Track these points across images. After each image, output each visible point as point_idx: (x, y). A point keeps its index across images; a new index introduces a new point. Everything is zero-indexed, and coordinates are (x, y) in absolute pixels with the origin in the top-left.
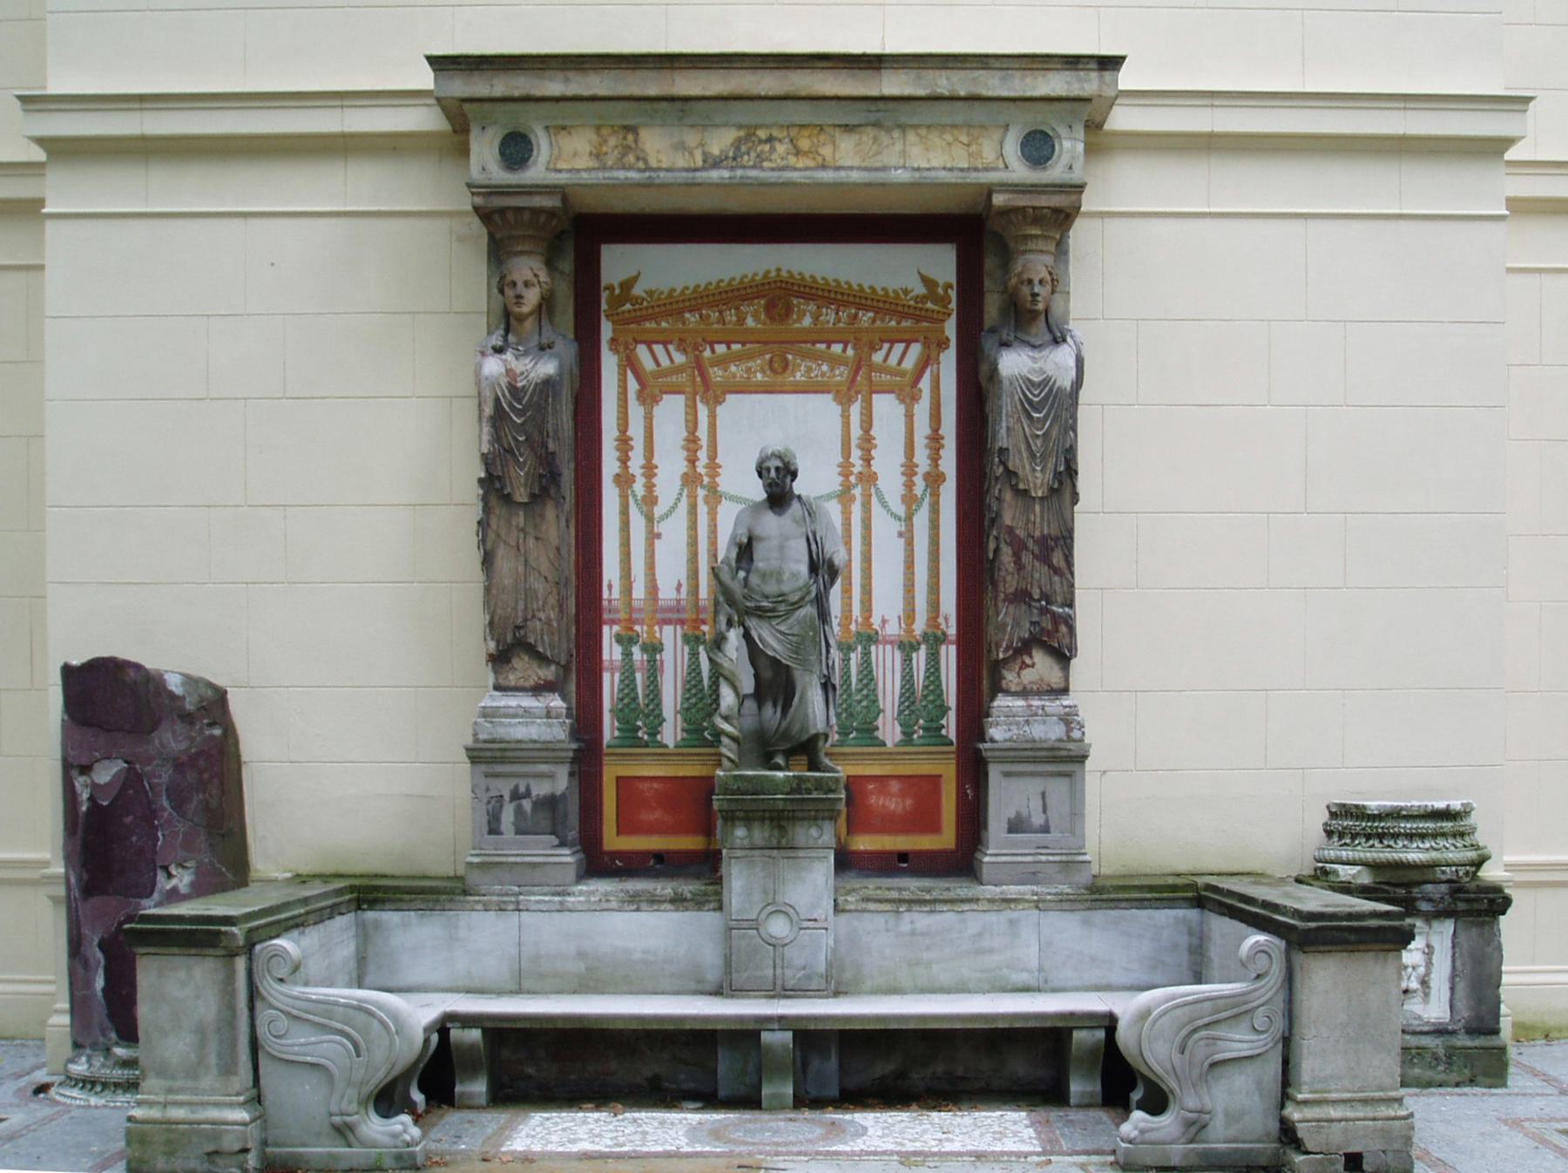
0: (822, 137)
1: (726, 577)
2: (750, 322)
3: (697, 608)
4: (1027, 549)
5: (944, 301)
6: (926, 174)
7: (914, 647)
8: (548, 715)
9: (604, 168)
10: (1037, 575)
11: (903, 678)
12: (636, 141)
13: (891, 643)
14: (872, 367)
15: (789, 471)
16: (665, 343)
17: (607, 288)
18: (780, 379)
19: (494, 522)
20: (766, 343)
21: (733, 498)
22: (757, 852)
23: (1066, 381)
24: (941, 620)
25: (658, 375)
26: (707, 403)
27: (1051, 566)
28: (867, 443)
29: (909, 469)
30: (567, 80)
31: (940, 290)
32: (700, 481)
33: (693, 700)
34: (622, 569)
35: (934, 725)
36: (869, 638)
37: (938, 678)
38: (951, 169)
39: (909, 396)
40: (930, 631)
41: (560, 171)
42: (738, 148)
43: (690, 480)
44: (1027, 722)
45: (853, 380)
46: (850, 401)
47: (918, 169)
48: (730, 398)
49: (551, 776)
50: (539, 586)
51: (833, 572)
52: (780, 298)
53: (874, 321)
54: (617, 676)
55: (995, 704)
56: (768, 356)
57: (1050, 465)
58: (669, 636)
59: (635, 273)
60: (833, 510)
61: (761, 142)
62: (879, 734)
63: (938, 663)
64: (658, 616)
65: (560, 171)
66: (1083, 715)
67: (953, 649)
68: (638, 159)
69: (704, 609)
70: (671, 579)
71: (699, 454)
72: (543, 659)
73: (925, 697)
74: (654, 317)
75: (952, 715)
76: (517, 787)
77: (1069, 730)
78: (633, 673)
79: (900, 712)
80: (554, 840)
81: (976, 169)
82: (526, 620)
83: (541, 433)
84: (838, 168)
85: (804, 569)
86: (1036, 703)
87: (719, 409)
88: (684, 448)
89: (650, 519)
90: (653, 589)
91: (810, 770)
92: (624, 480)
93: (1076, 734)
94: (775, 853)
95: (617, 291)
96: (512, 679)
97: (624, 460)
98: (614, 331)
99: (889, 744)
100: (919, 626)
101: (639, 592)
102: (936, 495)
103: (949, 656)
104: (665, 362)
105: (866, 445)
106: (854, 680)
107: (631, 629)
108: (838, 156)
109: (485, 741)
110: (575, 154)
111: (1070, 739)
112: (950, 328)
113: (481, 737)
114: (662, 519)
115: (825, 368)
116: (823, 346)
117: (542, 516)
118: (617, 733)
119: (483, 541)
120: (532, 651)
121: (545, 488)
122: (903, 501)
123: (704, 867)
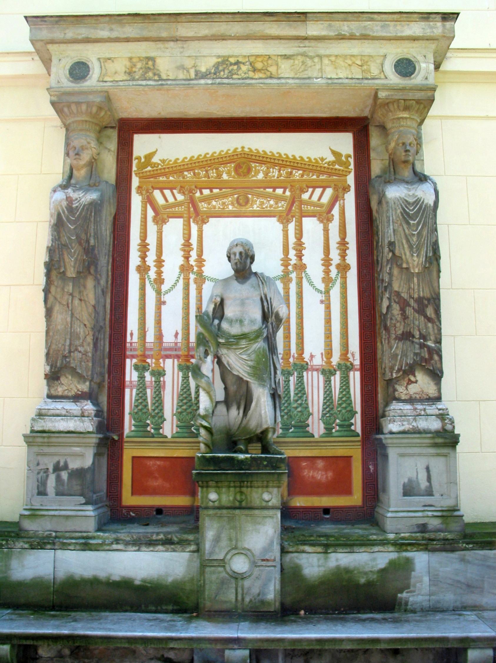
2: (225, 177)
3: (189, 349)
4: (409, 306)
5: (346, 164)
7: (332, 373)
9: (134, 80)
10: (417, 323)
11: (325, 392)
12: (154, 65)
13: (317, 370)
14: (302, 202)
16: (171, 189)
17: (136, 158)
18: (243, 209)
19: (53, 289)
20: (235, 188)
21: (212, 280)
22: (225, 511)
23: (430, 200)
24: (349, 355)
25: (165, 207)
26: (197, 223)
27: (426, 317)
28: (300, 247)
29: (327, 262)
30: (111, 30)
31: (343, 158)
32: (192, 269)
33: (184, 407)
34: (140, 324)
35: (347, 423)
36: (302, 367)
37: (349, 392)
38: (352, 79)
39: (325, 217)
40: (342, 362)
41: (106, 82)
42: (217, 68)
43: (185, 269)
44: (415, 420)
45: (290, 210)
46: (288, 221)
47: (330, 79)
49: (82, 455)
50: (80, 330)
51: (279, 320)
52: (244, 163)
53: (302, 176)
54: (134, 391)
55: (392, 408)
56: (236, 196)
57: (423, 253)
58: (170, 366)
59: (154, 150)
60: (280, 286)
61: (231, 64)
62: (310, 429)
64: (163, 353)
65: (106, 82)
66: (452, 414)
67: (358, 374)
70: (172, 327)
71: (191, 253)
72: (81, 378)
73: (340, 405)
74: (165, 174)
75: (358, 417)
76: (58, 462)
78: (145, 389)
79: (324, 415)
80: (82, 500)
81: (367, 79)
82: (70, 352)
83: (86, 234)
84: (279, 78)
85: (258, 315)
86: (419, 407)
87: (205, 227)
89: (159, 292)
90: (159, 336)
91: (262, 453)
92: (143, 269)
93: (449, 427)
95: (143, 160)
96: (60, 390)
97: (143, 257)
98: (140, 182)
99: (316, 436)
100: (335, 359)
101: (150, 337)
102: (344, 278)
103: (355, 378)
104: (171, 200)
106: (292, 394)
107: (145, 361)
108: (279, 72)
110: (116, 73)
112: (351, 180)
113: (36, 428)
114: (166, 292)
115: (272, 202)
116: (271, 190)
117: (85, 287)
119: (46, 301)
120: (74, 372)
121: (89, 266)
123: (190, 519)
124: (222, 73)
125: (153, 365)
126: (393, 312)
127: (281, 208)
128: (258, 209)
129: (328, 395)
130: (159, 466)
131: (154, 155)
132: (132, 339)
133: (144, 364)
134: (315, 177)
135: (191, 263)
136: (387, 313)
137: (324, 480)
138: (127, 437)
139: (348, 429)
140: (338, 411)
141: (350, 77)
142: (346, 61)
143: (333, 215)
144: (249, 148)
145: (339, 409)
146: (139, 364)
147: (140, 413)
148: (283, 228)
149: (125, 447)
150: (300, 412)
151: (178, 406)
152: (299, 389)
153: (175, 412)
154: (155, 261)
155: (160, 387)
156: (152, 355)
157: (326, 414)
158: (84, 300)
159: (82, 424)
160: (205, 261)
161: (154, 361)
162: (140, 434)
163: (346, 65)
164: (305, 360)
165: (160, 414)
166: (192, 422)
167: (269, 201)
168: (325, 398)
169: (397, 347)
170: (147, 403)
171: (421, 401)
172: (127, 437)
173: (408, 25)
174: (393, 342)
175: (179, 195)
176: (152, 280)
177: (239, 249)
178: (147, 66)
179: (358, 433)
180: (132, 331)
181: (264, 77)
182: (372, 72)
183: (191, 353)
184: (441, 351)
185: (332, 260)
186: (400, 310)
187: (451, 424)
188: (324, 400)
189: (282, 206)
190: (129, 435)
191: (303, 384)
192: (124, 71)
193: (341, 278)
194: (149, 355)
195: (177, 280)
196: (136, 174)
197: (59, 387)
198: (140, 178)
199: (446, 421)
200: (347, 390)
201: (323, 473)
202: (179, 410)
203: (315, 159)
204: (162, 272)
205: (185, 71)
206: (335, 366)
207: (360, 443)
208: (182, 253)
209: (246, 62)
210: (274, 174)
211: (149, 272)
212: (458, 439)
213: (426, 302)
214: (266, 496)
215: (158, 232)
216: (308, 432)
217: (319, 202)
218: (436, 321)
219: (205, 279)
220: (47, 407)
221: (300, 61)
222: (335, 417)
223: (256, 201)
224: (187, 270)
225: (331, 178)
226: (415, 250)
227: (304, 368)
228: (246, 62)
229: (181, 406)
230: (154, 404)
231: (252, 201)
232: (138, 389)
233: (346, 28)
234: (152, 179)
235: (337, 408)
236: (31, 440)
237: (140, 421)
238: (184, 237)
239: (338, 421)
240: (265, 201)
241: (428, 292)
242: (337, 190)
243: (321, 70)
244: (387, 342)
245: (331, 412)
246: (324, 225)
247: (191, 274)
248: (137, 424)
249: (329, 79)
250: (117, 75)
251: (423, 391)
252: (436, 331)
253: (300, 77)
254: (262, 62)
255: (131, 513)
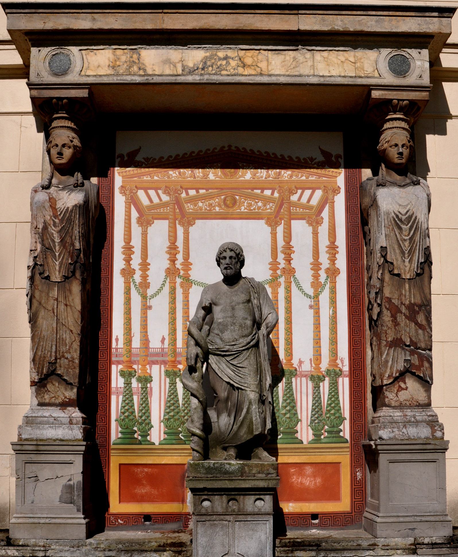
0: (260, 57)
1: (195, 331)
4: (401, 313)
6: (328, 79)
7: (321, 379)
8: (71, 423)
9: (118, 75)
11: (314, 399)
13: (305, 376)
14: (291, 204)
15: (239, 259)
16: (156, 189)
18: (231, 210)
19: (37, 294)
20: (222, 189)
21: (199, 284)
24: (339, 361)
25: (150, 208)
28: (288, 250)
29: (316, 266)
31: (333, 159)
32: (178, 273)
33: (172, 414)
34: (125, 329)
37: (338, 398)
38: (344, 77)
39: (314, 218)
40: (331, 368)
41: (88, 76)
43: (171, 272)
44: (405, 426)
45: (279, 211)
46: (277, 224)
47: (323, 76)
48: (199, 223)
50: (67, 336)
53: (291, 176)
54: (121, 398)
56: (223, 197)
58: (156, 372)
59: (137, 147)
61: (220, 59)
62: (298, 435)
63: (337, 389)
67: (347, 380)
68: (140, 69)
69: (180, 354)
70: (158, 333)
71: (177, 256)
75: (347, 424)
77: (433, 431)
78: (132, 395)
79: (312, 421)
81: (360, 77)
82: (56, 359)
86: (409, 413)
87: (191, 229)
88: (167, 252)
89: (144, 297)
90: (145, 340)
93: (438, 434)
94: (231, 518)
95: (126, 158)
96: (47, 398)
97: (128, 260)
99: (305, 442)
100: (324, 365)
101: (136, 343)
103: (344, 385)
104: (156, 200)
105: (288, 251)
107: (131, 367)
109: (27, 440)
111: (435, 438)
113: (24, 436)
114: (152, 297)
115: (260, 204)
116: (259, 191)
117: (70, 291)
118: (120, 435)
122: (312, 286)
124: (210, 69)
125: (140, 371)
126: (384, 318)
127: (269, 210)
128: (246, 210)
129: (317, 401)
130: (147, 473)
131: (138, 153)
132: (117, 345)
133: (130, 370)
134: (304, 178)
135: (177, 266)
136: (377, 319)
137: (312, 486)
138: (113, 444)
139: (337, 435)
140: (327, 417)
141: (343, 75)
142: (339, 57)
143: (322, 218)
144: (236, 147)
145: (328, 415)
146: (125, 370)
147: (127, 420)
148: (272, 231)
149: (111, 454)
150: (289, 418)
151: (165, 412)
152: (288, 395)
153: (162, 419)
154: (139, 265)
155: (147, 394)
156: (138, 361)
157: (315, 420)
158: (70, 306)
159: (70, 432)
160: (191, 264)
161: (140, 366)
162: (127, 441)
163: (339, 62)
164: (293, 366)
165: (147, 421)
166: (180, 429)
167: (256, 203)
168: (313, 405)
169: (388, 354)
170: (134, 409)
171: (410, 406)
172: (113, 444)
173: (404, 20)
174: (383, 348)
175: (165, 195)
176: (137, 284)
177: (228, 254)
178: (132, 59)
179: (347, 439)
180: (117, 336)
181: (253, 73)
182: (365, 69)
183: (178, 359)
184: (432, 358)
185: (321, 264)
186: (391, 317)
187: (440, 431)
188: (313, 406)
189: (271, 208)
190: (116, 442)
191: (292, 390)
192: (107, 64)
193: (330, 282)
194: (135, 361)
195: (164, 284)
196: (119, 173)
197: (45, 395)
198: (123, 177)
199: (436, 428)
200: (336, 396)
201: (312, 479)
202: (167, 417)
203: (304, 159)
204: (148, 276)
205: (172, 66)
206: (323, 372)
207: (348, 450)
208: (168, 256)
209: (236, 57)
210: (262, 174)
211: (134, 276)
212: (448, 445)
213: (417, 309)
214: (259, 503)
215: (142, 234)
216: (297, 438)
217: (308, 204)
218: (427, 327)
219: (192, 283)
220: (34, 415)
221: (292, 56)
222: (324, 423)
223: (244, 203)
224: (173, 273)
225: (321, 179)
226: (406, 255)
227: (320, 380)
228: (236, 57)
229: (168, 413)
230: (141, 410)
231: (240, 202)
232: (125, 396)
233: (340, 23)
234: (136, 179)
235: (326, 414)
236: (18, 448)
237: (127, 428)
238: (169, 240)
239: (326, 427)
240: (253, 203)
241: (419, 298)
242: (327, 192)
243: (313, 66)
244: (377, 348)
245: (320, 418)
246: (313, 228)
247: (177, 277)
248: (124, 431)
249: (321, 76)
250: (100, 68)
251: (413, 398)
252: (427, 338)
253: (291, 74)
254: (252, 57)
255: (119, 520)
